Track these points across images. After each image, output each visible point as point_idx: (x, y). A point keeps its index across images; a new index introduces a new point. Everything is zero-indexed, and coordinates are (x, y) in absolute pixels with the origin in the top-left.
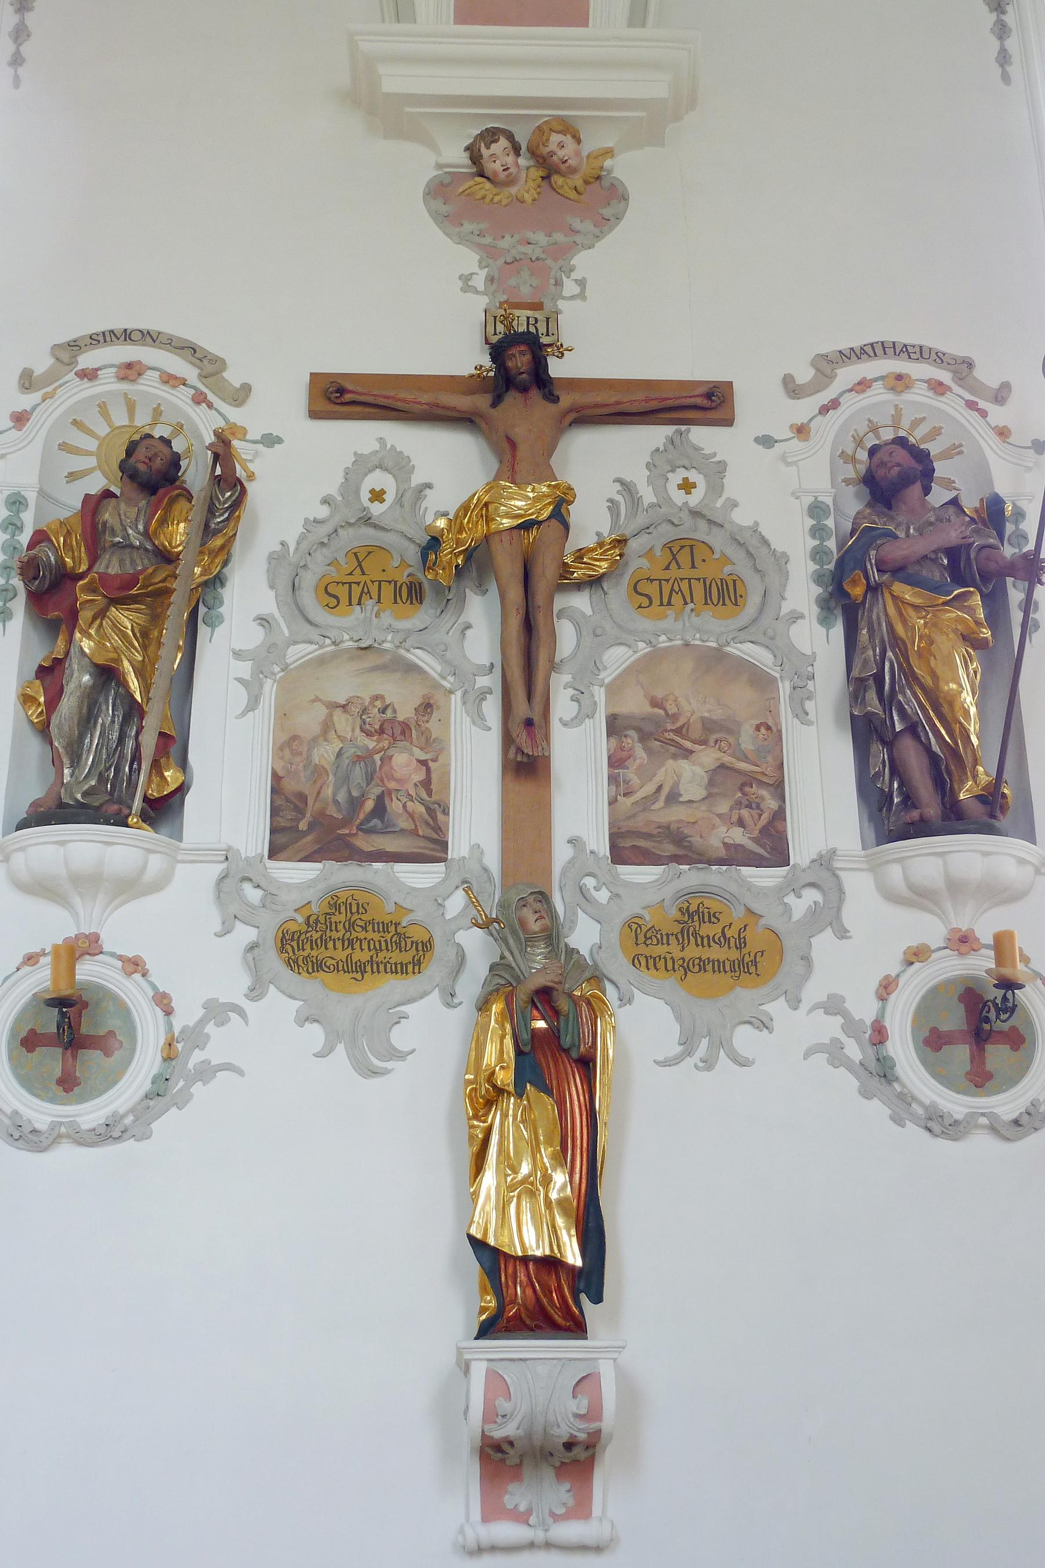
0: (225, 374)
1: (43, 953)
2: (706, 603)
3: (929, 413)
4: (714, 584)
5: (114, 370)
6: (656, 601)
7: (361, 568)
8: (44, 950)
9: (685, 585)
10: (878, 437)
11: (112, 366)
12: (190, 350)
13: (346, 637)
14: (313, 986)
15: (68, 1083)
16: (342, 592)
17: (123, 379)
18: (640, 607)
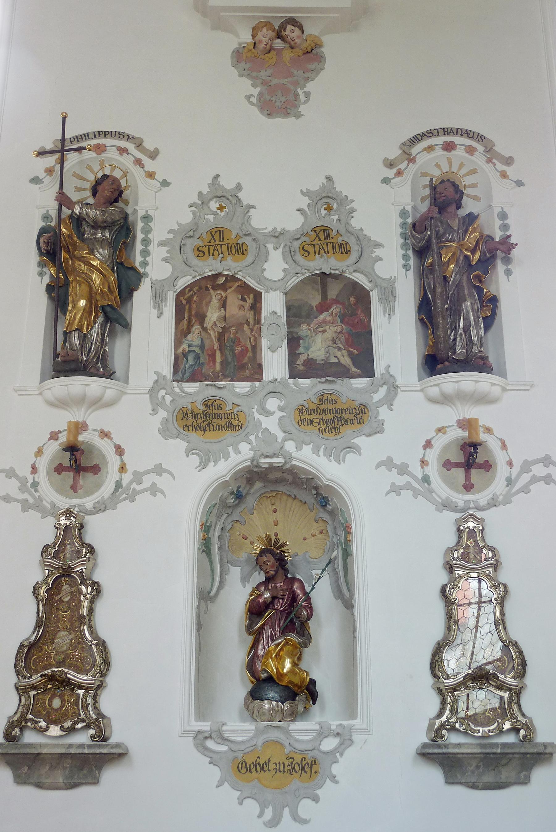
0: (495, 148)
2: (229, 254)
4: (233, 246)
5: (441, 146)
6: (207, 254)
7: (214, 239)
8: (390, 406)
9: (219, 247)
13: (207, 270)
14: (195, 436)
18: (303, 255)
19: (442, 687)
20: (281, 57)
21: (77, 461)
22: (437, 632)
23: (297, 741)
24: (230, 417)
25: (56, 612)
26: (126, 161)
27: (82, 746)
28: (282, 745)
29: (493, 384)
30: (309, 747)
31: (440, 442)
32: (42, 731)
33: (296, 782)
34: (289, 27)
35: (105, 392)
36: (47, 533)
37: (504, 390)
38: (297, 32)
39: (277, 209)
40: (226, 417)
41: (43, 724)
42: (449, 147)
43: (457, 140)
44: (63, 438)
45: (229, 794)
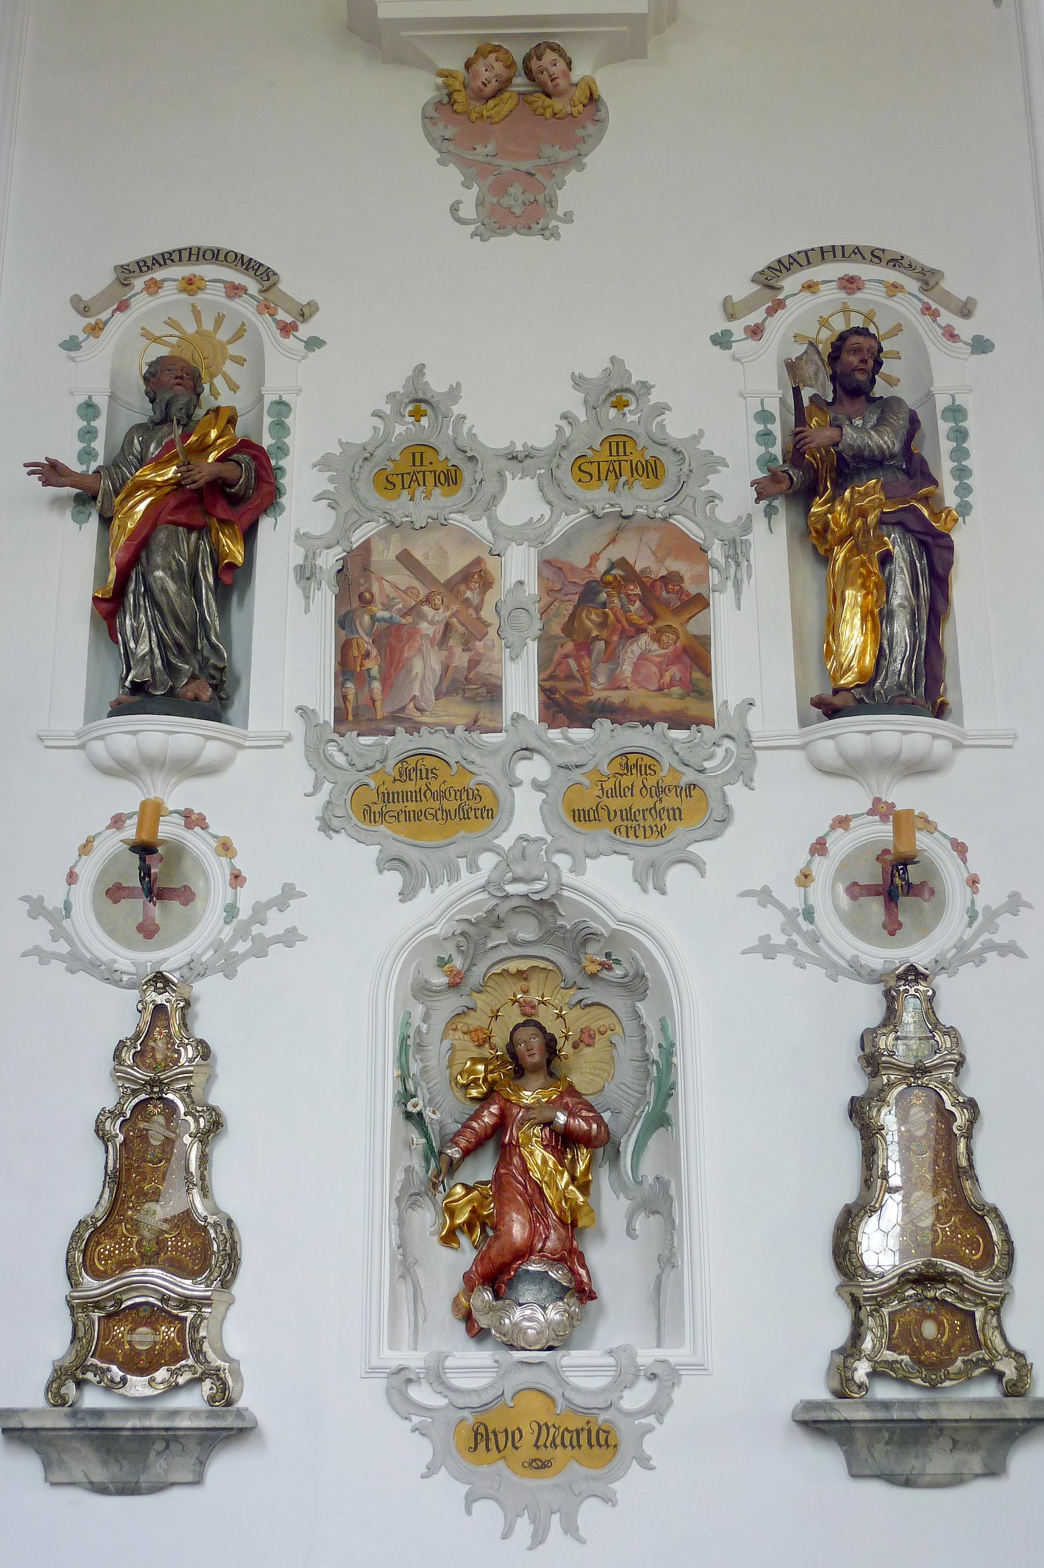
0: (280, 286)
1: (130, 816)
3: (889, 308)
9: (420, 476)
10: (831, 329)
11: (175, 280)
12: (247, 265)
15: (148, 931)
16: (398, 481)
17: (183, 290)
19: (858, 1293)
20: (517, 111)
21: (151, 874)
22: (848, 1192)
23: (577, 1390)
24: (464, 796)
25: (139, 1167)
26: (244, 308)
27: (195, 1413)
28: (552, 1399)
29: (935, 737)
30: (601, 1402)
31: (841, 844)
32: (111, 1387)
33: (573, 1469)
34: (549, 56)
35: (204, 747)
36: (119, 1015)
37: (957, 746)
38: (561, 65)
39: (515, 403)
40: (458, 797)
41: (116, 1372)
42: (191, 285)
43: (207, 271)
44: (130, 832)
45: (449, 1488)
